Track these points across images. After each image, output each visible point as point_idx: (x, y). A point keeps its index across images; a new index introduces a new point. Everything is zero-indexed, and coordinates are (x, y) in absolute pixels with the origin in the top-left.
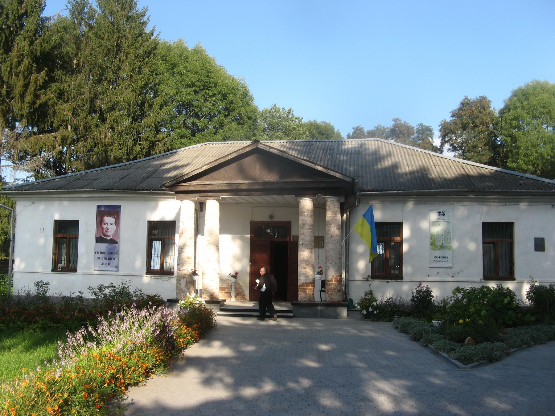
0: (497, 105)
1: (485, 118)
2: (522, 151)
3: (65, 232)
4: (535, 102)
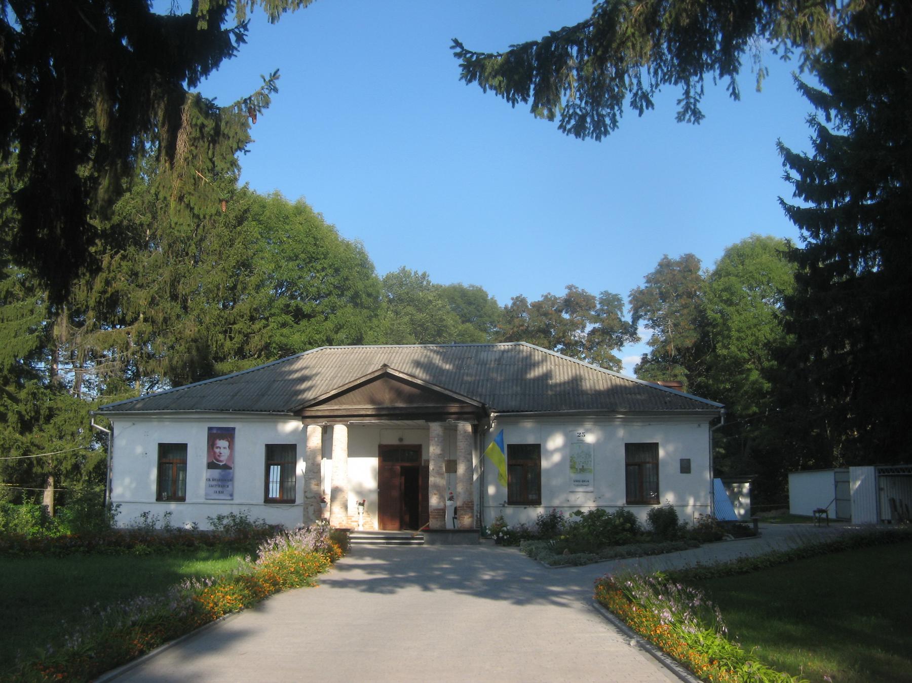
0: (708, 265)
1: (690, 285)
2: (734, 334)
3: (171, 457)
4: (751, 268)
